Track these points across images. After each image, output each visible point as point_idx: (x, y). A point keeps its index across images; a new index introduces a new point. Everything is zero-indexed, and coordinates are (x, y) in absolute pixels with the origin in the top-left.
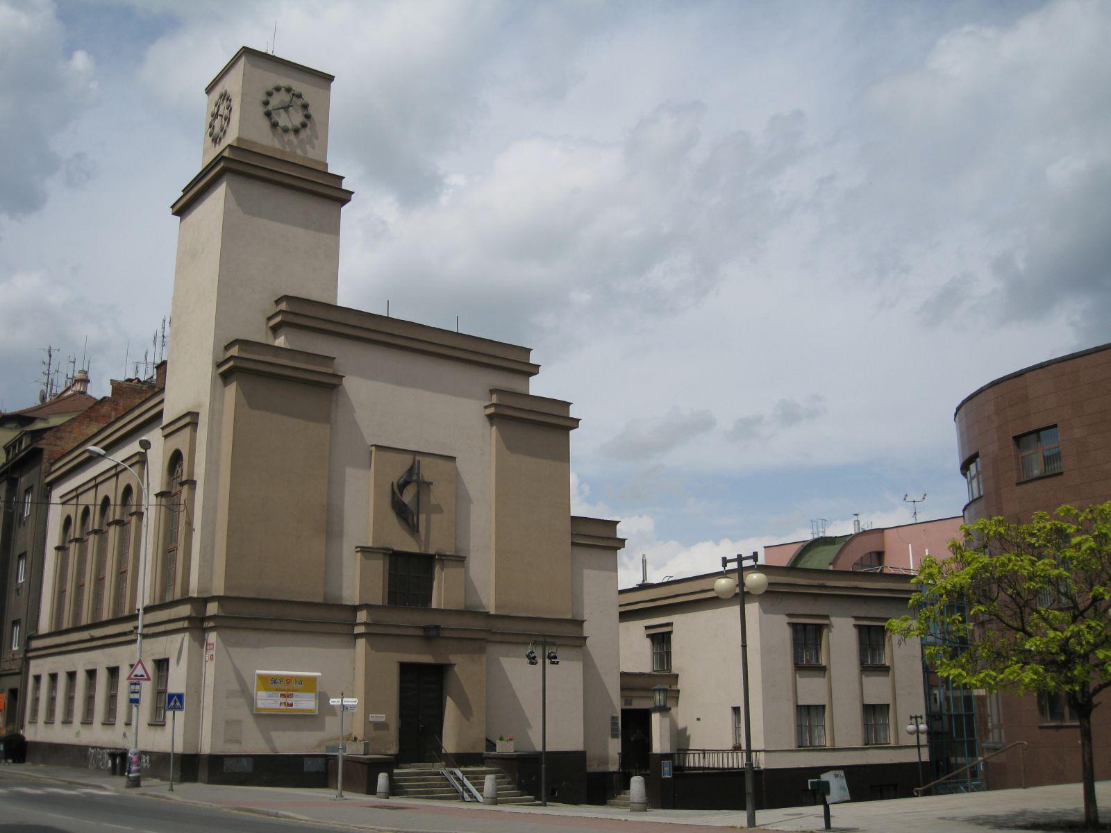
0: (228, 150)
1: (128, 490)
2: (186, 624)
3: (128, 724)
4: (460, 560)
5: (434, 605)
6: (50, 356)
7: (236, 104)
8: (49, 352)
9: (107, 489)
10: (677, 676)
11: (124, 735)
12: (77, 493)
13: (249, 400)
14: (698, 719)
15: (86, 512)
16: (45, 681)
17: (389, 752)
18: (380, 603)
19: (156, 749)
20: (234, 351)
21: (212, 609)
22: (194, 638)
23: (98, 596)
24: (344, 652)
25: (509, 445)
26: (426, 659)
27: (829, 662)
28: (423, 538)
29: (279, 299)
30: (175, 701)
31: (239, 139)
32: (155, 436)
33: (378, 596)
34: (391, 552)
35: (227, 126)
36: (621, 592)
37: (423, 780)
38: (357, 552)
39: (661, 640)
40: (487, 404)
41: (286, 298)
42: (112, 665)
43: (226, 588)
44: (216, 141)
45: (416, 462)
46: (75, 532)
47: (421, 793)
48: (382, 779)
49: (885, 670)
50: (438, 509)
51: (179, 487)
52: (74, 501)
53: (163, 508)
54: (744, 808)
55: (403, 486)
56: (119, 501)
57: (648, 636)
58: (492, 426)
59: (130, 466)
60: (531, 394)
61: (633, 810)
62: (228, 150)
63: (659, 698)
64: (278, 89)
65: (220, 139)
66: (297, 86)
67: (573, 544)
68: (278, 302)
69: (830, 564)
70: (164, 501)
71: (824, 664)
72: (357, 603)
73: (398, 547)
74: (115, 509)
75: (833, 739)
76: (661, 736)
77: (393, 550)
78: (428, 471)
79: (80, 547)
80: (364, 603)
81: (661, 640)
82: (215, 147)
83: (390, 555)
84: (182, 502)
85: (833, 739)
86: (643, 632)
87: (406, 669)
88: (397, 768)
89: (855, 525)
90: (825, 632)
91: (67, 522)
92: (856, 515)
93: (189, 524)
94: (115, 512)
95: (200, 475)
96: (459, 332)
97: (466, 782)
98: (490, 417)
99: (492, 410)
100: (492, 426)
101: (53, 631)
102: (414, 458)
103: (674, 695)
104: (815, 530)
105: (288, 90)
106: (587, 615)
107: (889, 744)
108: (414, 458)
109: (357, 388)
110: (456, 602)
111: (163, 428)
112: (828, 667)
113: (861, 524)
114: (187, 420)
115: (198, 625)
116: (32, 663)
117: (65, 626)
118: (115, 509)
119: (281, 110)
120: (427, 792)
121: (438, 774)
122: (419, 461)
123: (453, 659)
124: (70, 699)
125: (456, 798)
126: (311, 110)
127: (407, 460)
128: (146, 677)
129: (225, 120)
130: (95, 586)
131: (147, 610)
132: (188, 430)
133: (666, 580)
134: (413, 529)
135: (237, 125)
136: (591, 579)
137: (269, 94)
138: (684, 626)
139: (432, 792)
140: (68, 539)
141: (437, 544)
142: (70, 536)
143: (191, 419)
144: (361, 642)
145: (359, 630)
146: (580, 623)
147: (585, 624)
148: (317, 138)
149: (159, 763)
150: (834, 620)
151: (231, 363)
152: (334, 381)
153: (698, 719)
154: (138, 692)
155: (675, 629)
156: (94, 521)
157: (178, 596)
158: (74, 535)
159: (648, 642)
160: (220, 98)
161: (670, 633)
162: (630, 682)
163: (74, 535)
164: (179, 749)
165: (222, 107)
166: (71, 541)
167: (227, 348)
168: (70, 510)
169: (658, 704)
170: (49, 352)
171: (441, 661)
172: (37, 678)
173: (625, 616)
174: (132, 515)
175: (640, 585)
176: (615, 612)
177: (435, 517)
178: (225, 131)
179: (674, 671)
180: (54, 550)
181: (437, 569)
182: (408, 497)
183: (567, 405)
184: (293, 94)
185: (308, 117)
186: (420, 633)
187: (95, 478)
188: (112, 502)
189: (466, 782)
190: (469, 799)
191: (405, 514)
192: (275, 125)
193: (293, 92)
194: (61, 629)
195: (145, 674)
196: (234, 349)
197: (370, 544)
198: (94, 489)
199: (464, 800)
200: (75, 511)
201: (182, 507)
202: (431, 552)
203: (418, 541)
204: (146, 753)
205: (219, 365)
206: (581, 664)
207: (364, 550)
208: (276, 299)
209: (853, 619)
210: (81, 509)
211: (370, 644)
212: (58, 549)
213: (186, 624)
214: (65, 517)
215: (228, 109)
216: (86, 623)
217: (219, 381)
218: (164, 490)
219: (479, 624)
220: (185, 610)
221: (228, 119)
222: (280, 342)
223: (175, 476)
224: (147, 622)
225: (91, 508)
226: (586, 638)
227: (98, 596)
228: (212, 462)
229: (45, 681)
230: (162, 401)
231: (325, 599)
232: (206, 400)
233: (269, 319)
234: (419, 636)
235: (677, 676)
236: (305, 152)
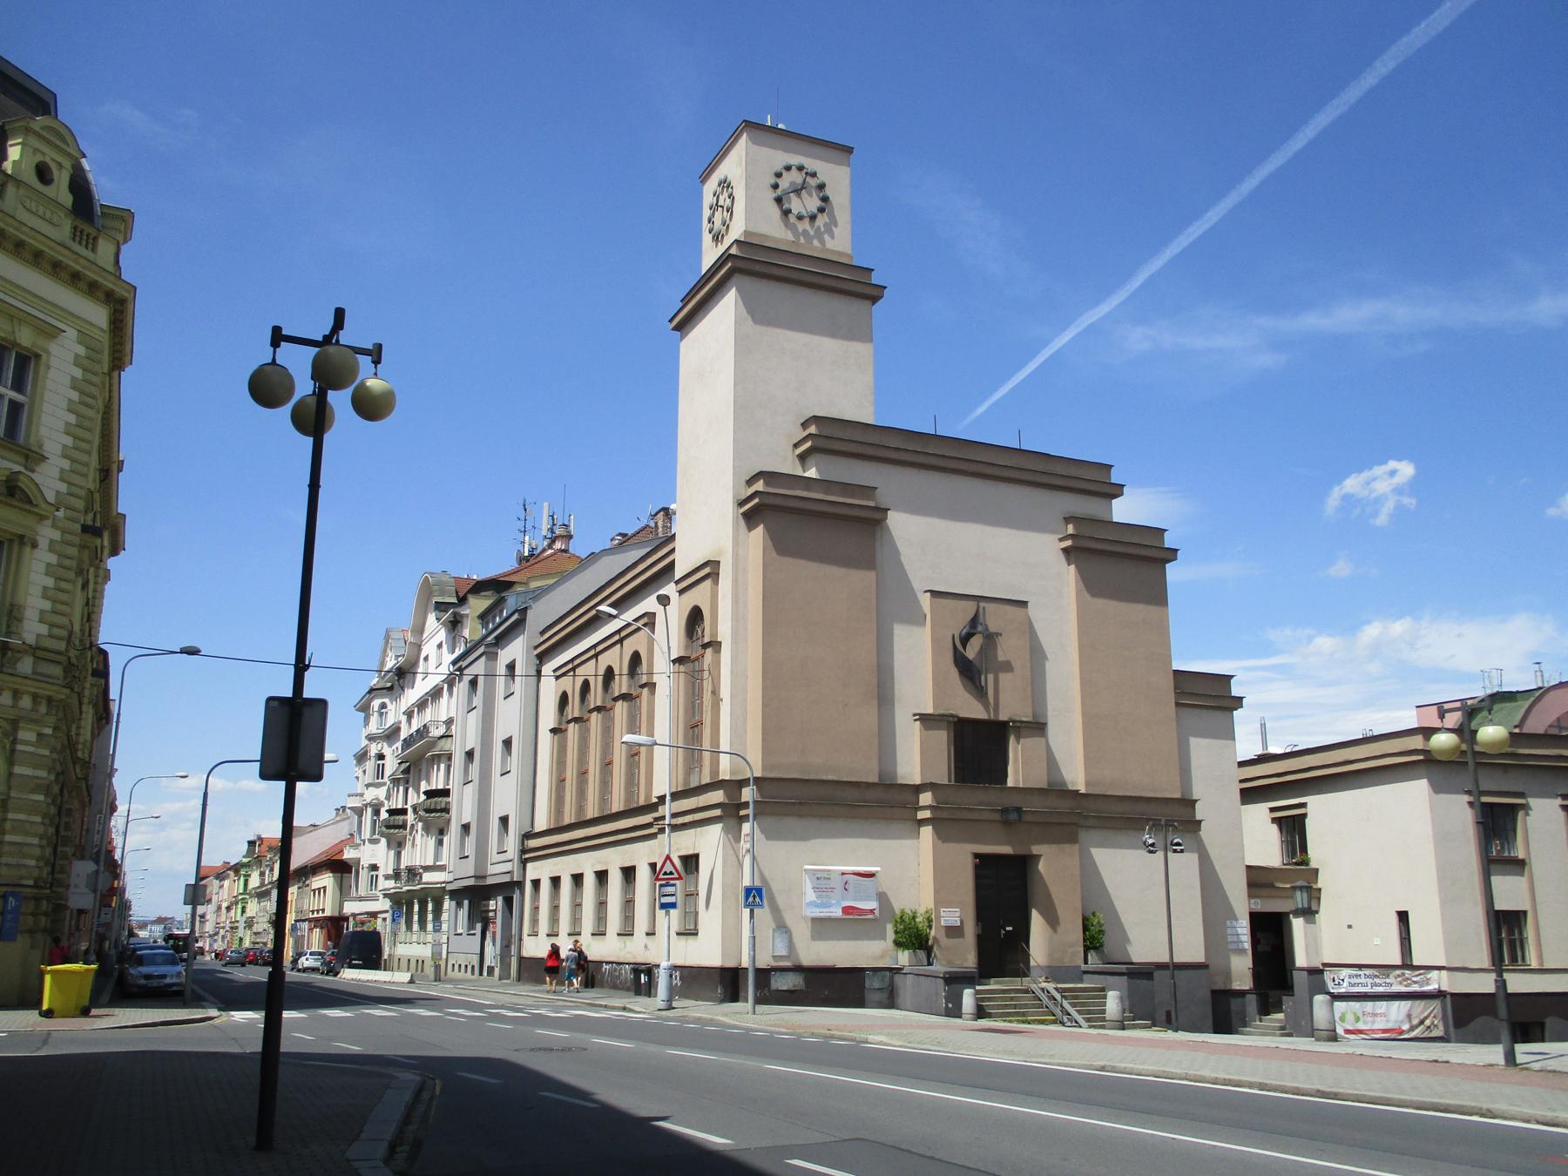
0: (735, 246)
1: (636, 659)
2: (718, 812)
3: (651, 934)
4: (1038, 727)
5: (1010, 783)
6: (526, 510)
7: (740, 193)
8: (524, 505)
9: (611, 658)
10: (1316, 871)
11: (646, 947)
12: (572, 667)
13: (780, 545)
14: (1350, 927)
15: (586, 687)
16: (545, 886)
17: (966, 965)
18: (946, 782)
19: (689, 963)
20: (759, 486)
21: (747, 794)
22: (726, 830)
23: (605, 785)
24: (908, 843)
25: (1092, 585)
26: (1006, 849)
27: (1528, 853)
28: (991, 701)
29: (807, 420)
30: (754, 896)
31: (746, 233)
32: (670, 589)
33: (942, 773)
34: (956, 719)
35: (731, 219)
36: (1242, 764)
37: (1012, 999)
38: (915, 720)
39: (1293, 829)
40: (1061, 536)
41: (816, 419)
42: (627, 864)
43: (764, 768)
44: (718, 238)
45: (981, 609)
46: (574, 709)
47: (1009, 1014)
48: (968, 998)
49: (1518, 865)
50: (1007, 667)
51: (700, 651)
52: (572, 673)
53: (682, 675)
54: (1496, 1041)
55: (965, 639)
56: (625, 671)
57: (1274, 820)
58: (1069, 565)
59: (643, 625)
60: (1114, 520)
61: (1318, 1040)
62: (735, 246)
63: (1300, 899)
64: (788, 168)
65: (723, 236)
66: (811, 164)
67: (1177, 704)
68: (805, 425)
69: (1516, 727)
70: (682, 668)
71: (1521, 856)
72: (918, 782)
73: (965, 713)
74: (620, 680)
75: (1540, 957)
76: (1307, 946)
77: (957, 717)
78: (994, 619)
79: (580, 728)
80: (928, 781)
81: (1293, 829)
82: (716, 246)
83: (955, 723)
84: (706, 667)
85: (1540, 957)
86: (1267, 816)
87: (984, 863)
88: (979, 985)
89: (1536, 677)
90: (1521, 814)
91: (564, 700)
92: (1538, 663)
93: (715, 692)
94: (621, 685)
95: (724, 633)
96: (1022, 448)
97: (1066, 1004)
98: (1066, 551)
99: (1069, 543)
100: (1069, 565)
101: (552, 827)
102: (978, 605)
103: (1314, 894)
104: (1487, 683)
105: (801, 168)
106: (1197, 792)
107: (1530, 965)
108: (978, 605)
109: (901, 524)
110: (1039, 780)
111: (677, 582)
112: (1527, 861)
113: (1546, 675)
114: (707, 570)
115: (732, 813)
116: (529, 866)
117: (567, 821)
118: (620, 680)
119: (792, 194)
120: (1017, 1014)
121: (1026, 991)
122: (984, 608)
123: (1036, 849)
124: (555, 908)
125: (1054, 1022)
126: (828, 191)
127: (969, 608)
128: (676, 875)
129: (728, 211)
130: (601, 773)
131: (676, 796)
132: (708, 583)
133: (1288, 750)
134: (979, 691)
135: (743, 215)
136: (1200, 748)
137: (779, 175)
138: (1321, 810)
139: (1024, 1014)
140: (564, 719)
141: (1011, 707)
142: (567, 715)
143: (710, 571)
144: (927, 832)
145: (922, 815)
146: (1192, 803)
147: (1198, 805)
148: (836, 226)
149: (693, 980)
150: (1533, 802)
151: (756, 500)
152: (877, 516)
153: (1350, 927)
154: (673, 895)
155: (1310, 810)
156: (596, 697)
157: (706, 780)
158: (572, 714)
159: (1275, 827)
160: (719, 185)
161: (1304, 816)
162: (1258, 879)
163: (572, 714)
164: (716, 961)
165: (721, 199)
166: (569, 722)
167: (750, 482)
168: (567, 683)
169: (1300, 906)
170: (524, 505)
171: (1022, 851)
172: (536, 883)
173: (1250, 795)
174: (643, 686)
175: (1259, 756)
176: (1235, 789)
177: (1002, 676)
178: (728, 225)
179: (1313, 865)
180: (549, 733)
181: (1012, 740)
182: (971, 652)
183: (1160, 532)
184: (806, 173)
185: (825, 199)
186: (997, 817)
187: (595, 646)
188: (617, 671)
189: (1066, 1004)
190: (1069, 1024)
191: (969, 672)
192: (786, 213)
193: (805, 170)
194: (561, 825)
195: (674, 871)
196: (758, 484)
197: (930, 710)
198: (594, 660)
199: (1063, 1024)
200: (571, 685)
201: (706, 674)
202: (1003, 717)
203: (986, 706)
204: (676, 967)
205: (741, 504)
206: (1196, 855)
207: (924, 719)
208: (802, 421)
209: (1559, 799)
210: (579, 681)
211: (936, 831)
212: (554, 731)
213: (718, 812)
214: (560, 693)
215: (730, 198)
216: (592, 817)
217: (742, 522)
218: (682, 654)
219: (1064, 805)
220: (717, 796)
221: (730, 210)
222: (812, 473)
223: (694, 639)
224: (675, 810)
225: (592, 680)
226: (1200, 822)
227: (605, 785)
228: (738, 618)
229: (545, 886)
230: (673, 550)
231: (880, 777)
232: (727, 544)
233: (796, 446)
234: (996, 821)
235: (1316, 871)
236: (822, 242)
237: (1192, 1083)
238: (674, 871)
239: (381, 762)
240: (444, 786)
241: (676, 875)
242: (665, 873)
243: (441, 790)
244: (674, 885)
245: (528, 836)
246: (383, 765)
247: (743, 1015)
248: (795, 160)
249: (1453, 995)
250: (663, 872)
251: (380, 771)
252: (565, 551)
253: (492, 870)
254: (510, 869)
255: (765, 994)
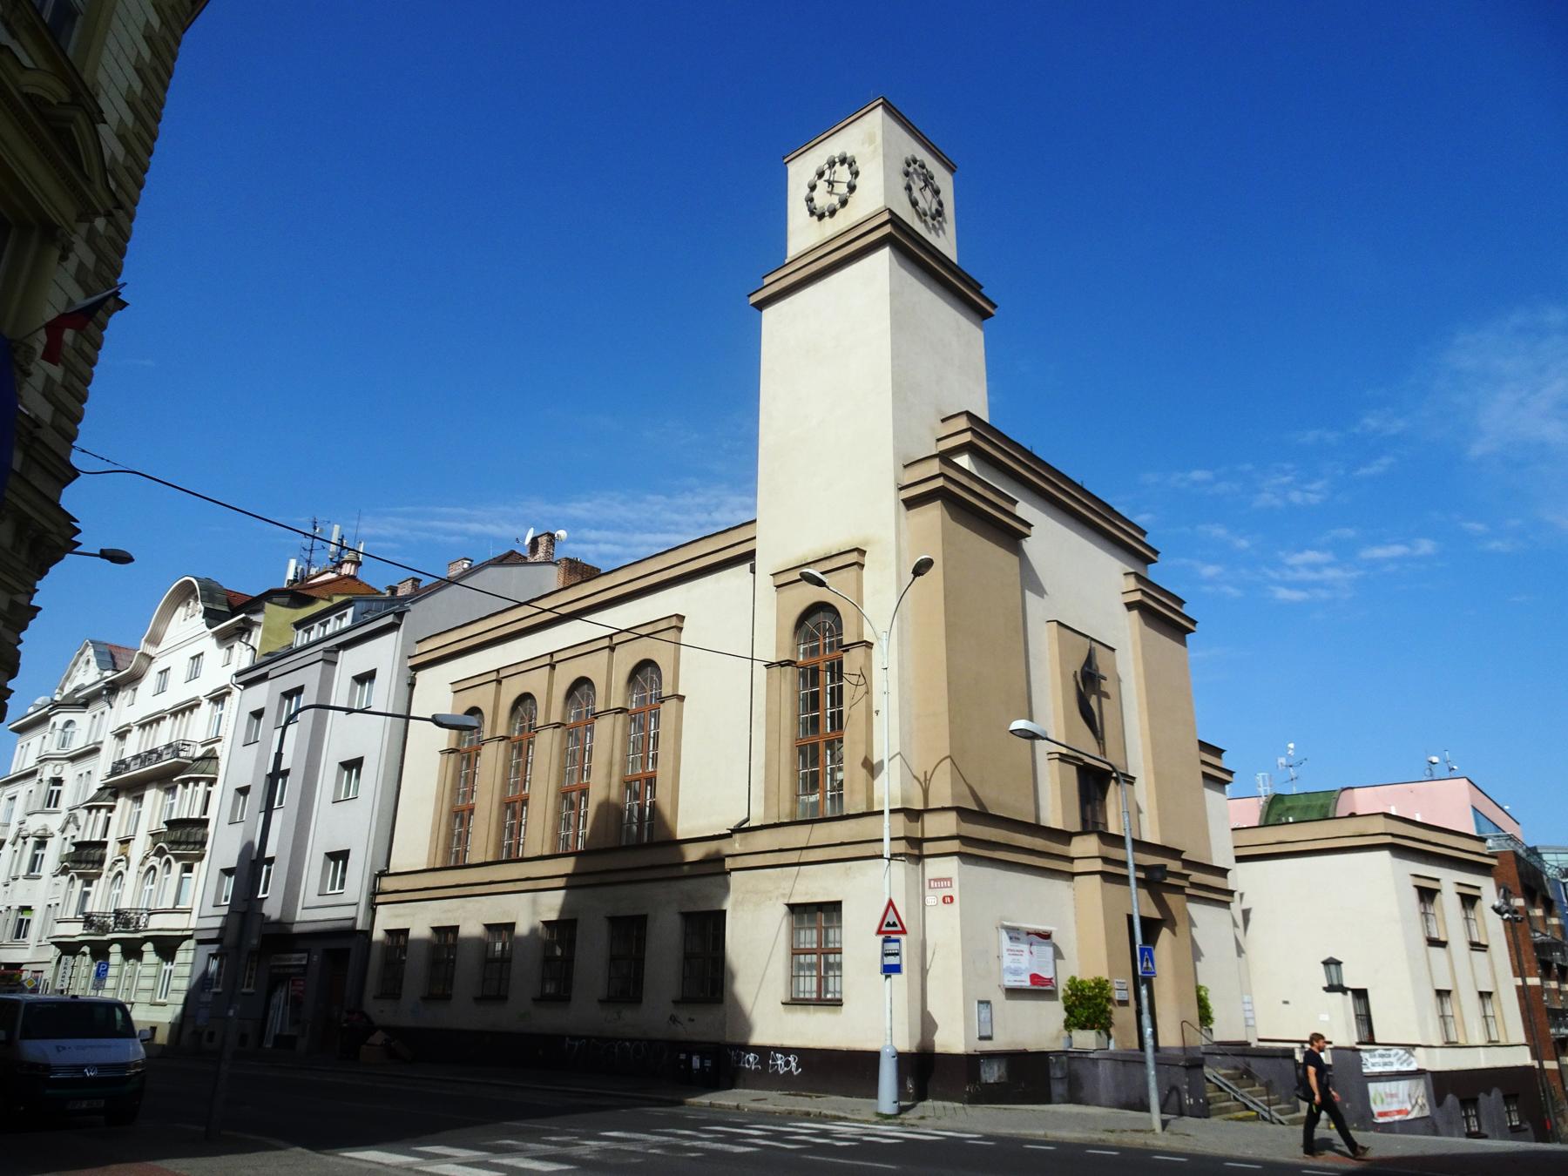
154: (897, 954)
161: (1478, 897)
195: (897, 922)
237: (1314, 1172)
238: (897, 922)
239: (56, 788)
240: (200, 815)
241: (899, 928)
242: (888, 925)
243: (185, 819)
244: (898, 941)
245: (383, 874)
246: (59, 792)
247: (842, 1114)
248: (844, 219)
249: (1433, 1073)
250: (885, 923)
251: (52, 800)
252: (353, 577)
253: (300, 915)
254: (353, 915)
255: (977, 1089)
